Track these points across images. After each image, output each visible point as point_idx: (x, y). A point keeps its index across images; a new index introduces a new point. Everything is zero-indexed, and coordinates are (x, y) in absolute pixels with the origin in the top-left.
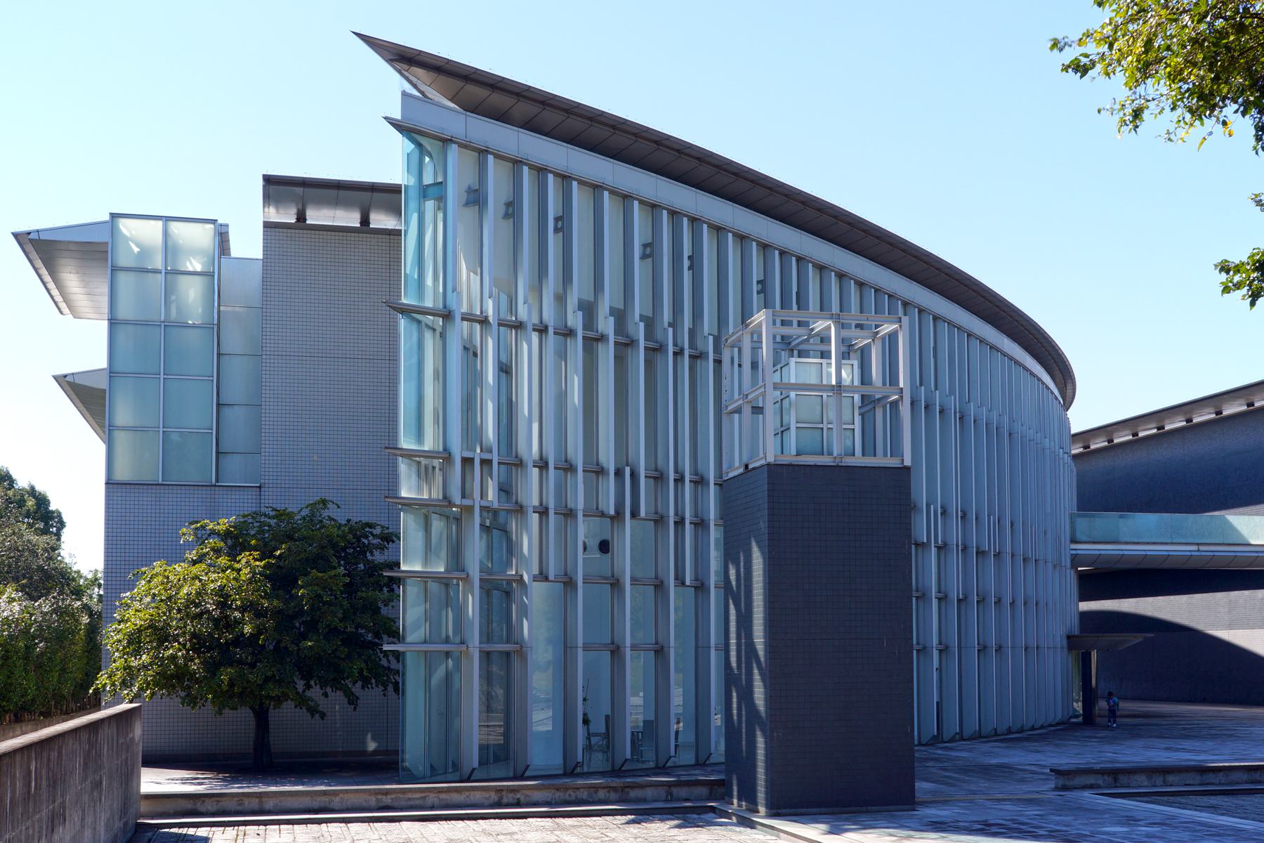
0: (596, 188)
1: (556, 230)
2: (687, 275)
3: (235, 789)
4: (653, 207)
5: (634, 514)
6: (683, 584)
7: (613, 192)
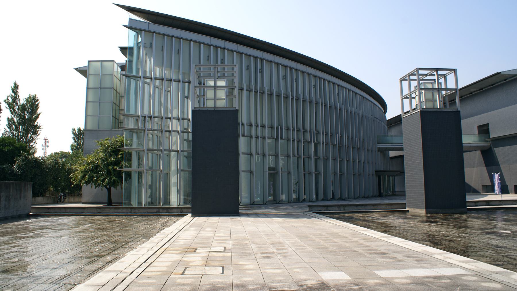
0: (303, 72)
1: (260, 72)
2: (337, 97)
3: (175, 164)
4: (315, 77)
5: (281, 138)
6: (295, 156)
7: (282, 65)
